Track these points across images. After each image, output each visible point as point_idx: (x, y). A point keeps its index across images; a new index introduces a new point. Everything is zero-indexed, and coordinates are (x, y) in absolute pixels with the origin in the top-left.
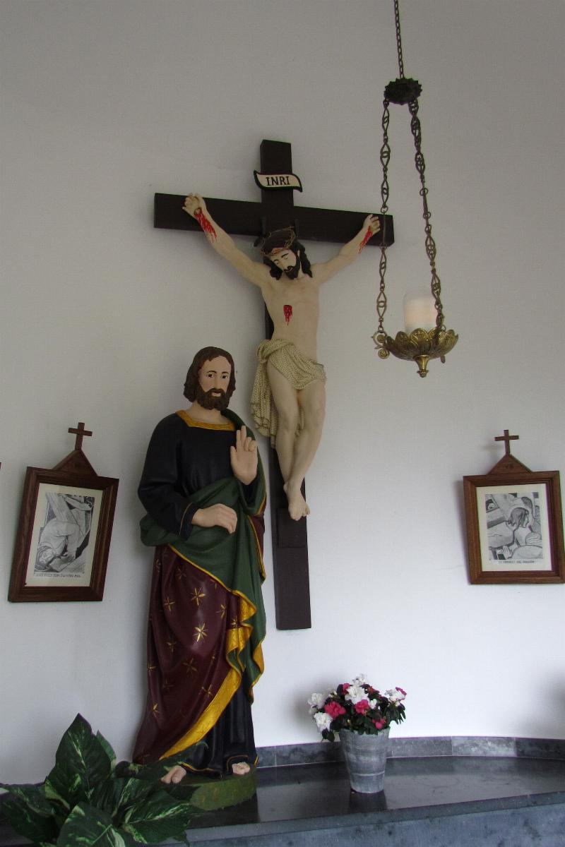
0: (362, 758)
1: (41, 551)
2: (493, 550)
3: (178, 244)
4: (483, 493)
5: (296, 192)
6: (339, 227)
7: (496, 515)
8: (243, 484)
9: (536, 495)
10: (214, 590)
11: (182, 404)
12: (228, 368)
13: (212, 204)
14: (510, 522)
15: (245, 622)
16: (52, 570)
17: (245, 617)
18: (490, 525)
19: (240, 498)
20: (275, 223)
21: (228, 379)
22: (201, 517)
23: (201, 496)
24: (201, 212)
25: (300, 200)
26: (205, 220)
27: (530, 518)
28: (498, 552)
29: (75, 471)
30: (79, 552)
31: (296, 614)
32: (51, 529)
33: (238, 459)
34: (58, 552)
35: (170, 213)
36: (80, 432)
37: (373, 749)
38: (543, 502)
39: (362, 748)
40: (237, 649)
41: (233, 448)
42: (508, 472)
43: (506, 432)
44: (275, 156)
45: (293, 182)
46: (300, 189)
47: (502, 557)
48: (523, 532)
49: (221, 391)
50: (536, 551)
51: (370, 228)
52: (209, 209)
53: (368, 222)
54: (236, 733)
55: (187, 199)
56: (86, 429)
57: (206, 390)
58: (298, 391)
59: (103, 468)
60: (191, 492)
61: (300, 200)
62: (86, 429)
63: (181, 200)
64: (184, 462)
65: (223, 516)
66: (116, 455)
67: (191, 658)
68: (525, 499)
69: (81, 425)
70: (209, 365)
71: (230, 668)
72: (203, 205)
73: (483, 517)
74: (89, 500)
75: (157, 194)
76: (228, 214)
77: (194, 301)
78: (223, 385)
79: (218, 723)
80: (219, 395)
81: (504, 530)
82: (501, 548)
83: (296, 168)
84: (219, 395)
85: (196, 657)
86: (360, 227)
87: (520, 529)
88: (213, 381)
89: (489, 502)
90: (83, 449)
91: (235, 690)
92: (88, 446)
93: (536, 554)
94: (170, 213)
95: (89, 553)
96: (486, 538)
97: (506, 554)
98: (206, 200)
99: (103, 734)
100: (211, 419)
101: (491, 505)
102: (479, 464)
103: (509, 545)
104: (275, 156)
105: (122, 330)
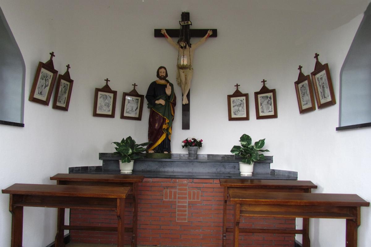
0: (191, 152)
1: (127, 109)
2: (234, 113)
3: (159, 41)
4: (232, 99)
5: (190, 26)
6: (201, 33)
7: (235, 104)
8: (168, 96)
9: (243, 99)
10: (160, 117)
11: (155, 79)
12: (165, 71)
13: (167, 31)
14: (238, 106)
15: (167, 123)
16: (129, 113)
17: (166, 122)
18: (233, 107)
19: (167, 99)
20: (185, 34)
21: (165, 73)
22: (157, 102)
23: (158, 98)
24: (165, 34)
25: (191, 27)
26: (166, 35)
27: (242, 105)
28: (235, 113)
29: (134, 93)
30: (136, 110)
31: (186, 126)
32: (129, 105)
33: (167, 90)
34: (131, 110)
35: (158, 33)
36: (135, 85)
37: (193, 150)
38: (245, 101)
39: (190, 150)
40: (165, 128)
41: (166, 88)
42: (238, 94)
43: (237, 84)
44: (186, 16)
45: (189, 23)
46: (191, 24)
47: (236, 114)
48: (240, 108)
49: (163, 76)
50: (243, 113)
51: (209, 33)
52: (167, 32)
53: (209, 32)
54: (165, 146)
55: (162, 30)
56: (136, 84)
57: (160, 76)
58: (186, 75)
59: (140, 93)
60: (156, 97)
61: (191, 27)
62: (136, 84)
63: (160, 30)
64: (156, 90)
65: (162, 102)
66: (143, 90)
67: (159, 130)
68: (241, 101)
69: (107, 79)
70: (160, 70)
71: (164, 133)
72: (165, 31)
73: (232, 105)
74: (138, 100)
75: (155, 30)
76: (172, 33)
77: (165, 54)
78: (164, 74)
79: (161, 143)
80: (163, 77)
81: (236, 108)
82: (236, 112)
83: (190, 20)
84: (163, 77)
85: (156, 129)
86: (207, 33)
87: (240, 108)
88: (162, 73)
89: (233, 101)
90: (108, 84)
91: (165, 137)
92: (109, 84)
93: (243, 113)
94: (158, 33)
95: (138, 110)
96: (233, 110)
97: (237, 114)
98: (166, 30)
99: (135, 140)
100: (163, 82)
101: (234, 102)
102: (232, 91)
103: (237, 111)
104: (186, 16)
105: (142, 61)
